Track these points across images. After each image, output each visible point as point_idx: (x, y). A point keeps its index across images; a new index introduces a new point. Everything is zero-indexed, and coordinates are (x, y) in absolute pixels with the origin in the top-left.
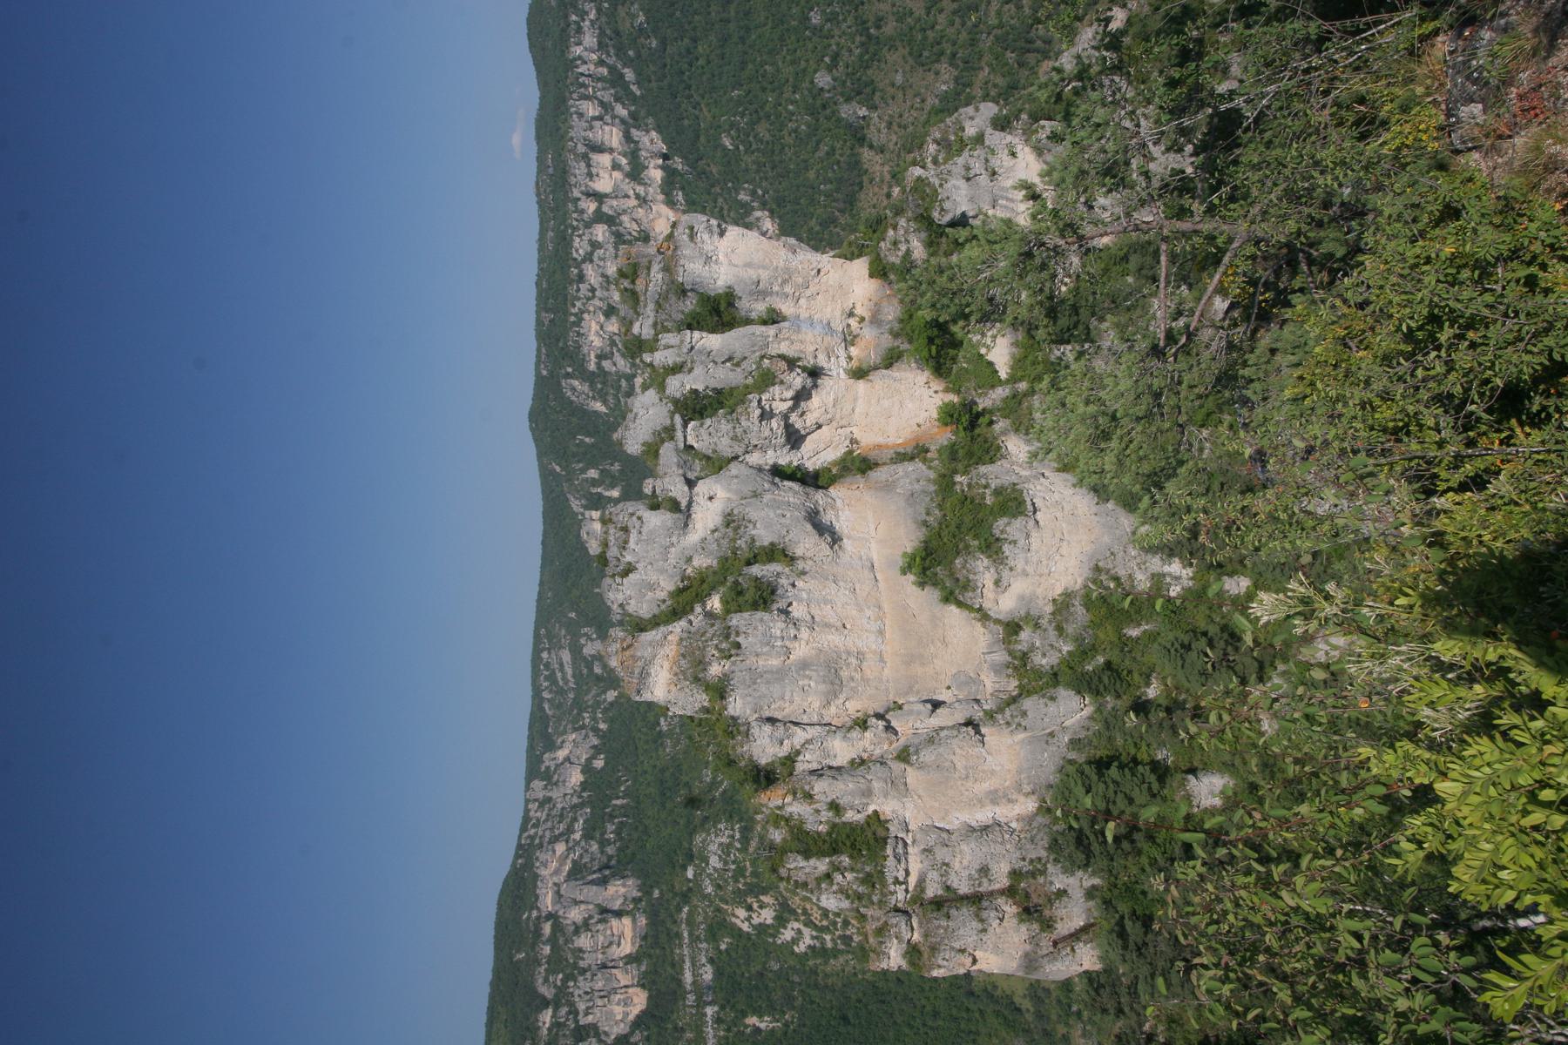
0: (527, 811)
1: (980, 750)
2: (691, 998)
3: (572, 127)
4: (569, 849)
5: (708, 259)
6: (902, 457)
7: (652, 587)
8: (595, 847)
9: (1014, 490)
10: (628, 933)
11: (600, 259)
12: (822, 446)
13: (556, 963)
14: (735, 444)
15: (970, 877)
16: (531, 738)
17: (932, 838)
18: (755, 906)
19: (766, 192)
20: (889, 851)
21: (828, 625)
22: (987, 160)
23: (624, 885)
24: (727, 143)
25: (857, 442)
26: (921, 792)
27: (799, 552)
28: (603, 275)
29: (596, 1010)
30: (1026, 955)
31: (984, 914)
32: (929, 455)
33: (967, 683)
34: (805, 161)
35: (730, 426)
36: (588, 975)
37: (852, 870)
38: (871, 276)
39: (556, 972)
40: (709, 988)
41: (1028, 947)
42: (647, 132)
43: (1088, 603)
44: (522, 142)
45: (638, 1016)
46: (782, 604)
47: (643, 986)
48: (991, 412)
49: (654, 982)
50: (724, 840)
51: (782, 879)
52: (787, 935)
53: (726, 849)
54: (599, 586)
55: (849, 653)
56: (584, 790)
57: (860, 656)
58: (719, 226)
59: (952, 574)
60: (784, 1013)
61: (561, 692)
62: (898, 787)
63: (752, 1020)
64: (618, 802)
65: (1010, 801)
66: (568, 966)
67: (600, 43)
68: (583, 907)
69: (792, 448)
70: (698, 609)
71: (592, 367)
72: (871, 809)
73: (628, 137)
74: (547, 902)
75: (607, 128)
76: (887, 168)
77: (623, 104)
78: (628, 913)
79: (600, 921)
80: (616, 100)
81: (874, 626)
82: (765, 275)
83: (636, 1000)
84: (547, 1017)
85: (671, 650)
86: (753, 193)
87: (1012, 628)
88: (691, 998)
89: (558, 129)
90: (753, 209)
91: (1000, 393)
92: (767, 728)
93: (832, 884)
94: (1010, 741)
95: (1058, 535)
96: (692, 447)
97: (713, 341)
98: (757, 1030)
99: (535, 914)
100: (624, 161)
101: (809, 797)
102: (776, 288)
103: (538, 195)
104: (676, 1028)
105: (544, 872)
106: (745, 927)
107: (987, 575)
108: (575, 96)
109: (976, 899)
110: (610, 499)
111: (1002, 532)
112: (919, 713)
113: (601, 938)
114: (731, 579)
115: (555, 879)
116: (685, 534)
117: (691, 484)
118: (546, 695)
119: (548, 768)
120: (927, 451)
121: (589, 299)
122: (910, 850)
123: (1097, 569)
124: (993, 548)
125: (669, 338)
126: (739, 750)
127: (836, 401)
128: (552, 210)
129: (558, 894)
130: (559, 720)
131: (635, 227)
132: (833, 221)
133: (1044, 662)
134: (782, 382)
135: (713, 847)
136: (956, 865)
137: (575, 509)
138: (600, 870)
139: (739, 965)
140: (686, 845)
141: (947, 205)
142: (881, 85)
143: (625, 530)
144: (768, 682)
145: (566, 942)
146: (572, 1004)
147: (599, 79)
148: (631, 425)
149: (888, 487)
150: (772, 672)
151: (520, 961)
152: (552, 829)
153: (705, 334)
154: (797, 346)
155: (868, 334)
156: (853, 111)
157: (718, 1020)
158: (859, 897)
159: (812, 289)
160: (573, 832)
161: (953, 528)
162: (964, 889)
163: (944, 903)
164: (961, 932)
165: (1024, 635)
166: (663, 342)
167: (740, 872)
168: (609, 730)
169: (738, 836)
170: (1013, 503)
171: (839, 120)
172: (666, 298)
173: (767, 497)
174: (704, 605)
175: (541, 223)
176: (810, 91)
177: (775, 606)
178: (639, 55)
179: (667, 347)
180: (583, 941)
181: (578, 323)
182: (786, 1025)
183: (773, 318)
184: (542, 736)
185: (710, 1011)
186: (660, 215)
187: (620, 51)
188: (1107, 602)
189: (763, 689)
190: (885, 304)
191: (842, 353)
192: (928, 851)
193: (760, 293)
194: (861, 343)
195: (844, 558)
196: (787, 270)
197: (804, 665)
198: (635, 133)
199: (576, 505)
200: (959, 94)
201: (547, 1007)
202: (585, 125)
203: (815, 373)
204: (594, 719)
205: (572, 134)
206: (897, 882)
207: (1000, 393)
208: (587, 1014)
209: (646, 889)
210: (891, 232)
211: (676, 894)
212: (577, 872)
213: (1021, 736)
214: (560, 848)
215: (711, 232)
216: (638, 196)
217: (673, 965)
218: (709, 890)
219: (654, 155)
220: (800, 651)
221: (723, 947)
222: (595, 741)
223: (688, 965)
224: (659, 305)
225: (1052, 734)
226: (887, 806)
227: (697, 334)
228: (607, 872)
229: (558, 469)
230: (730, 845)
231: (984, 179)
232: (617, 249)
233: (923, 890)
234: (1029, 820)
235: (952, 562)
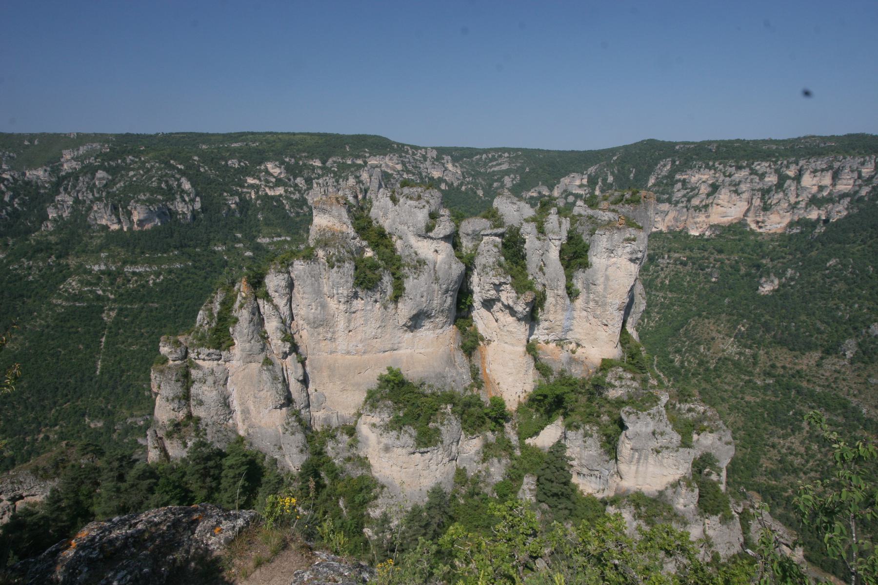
0: (421, 148)
3: (854, 158)
4: (398, 171)
6: (475, 373)
7: (385, 215)
9: (437, 441)
11: (752, 179)
13: (343, 167)
15: (198, 395)
16: (462, 149)
19: (792, 287)
20: (211, 351)
21: (349, 321)
22: (667, 448)
24: (832, 262)
25: (488, 344)
26: (246, 370)
27: (400, 305)
28: (740, 182)
32: (475, 389)
34: (814, 314)
36: (335, 184)
38: (603, 360)
39: (338, 167)
42: (847, 209)
43: (362, 478)
46: (360, 293)
48: (502, 431)
54: (543, 184)
55: (334, 333)
56: (429, 179)
57: (333, 339)
58: (637, 259)
59: (382, 398)
61: (485, 165)
62: (249, 358)
65: (244, 420)
70: (365, 243)
71: (678, 177)
73: (843, 196)
74: (373, 161)
75: (851, 182)
76: (805, 367)
77: (870, 192)
80: (873, 188)
82: (600, 288)
84: (317, 163)
85: (338, 227)
86: (792, 279)
87: (351, 431)
89: (854, 149)
90: (780, 278)
91: (514, 439)
94: (277, 424)
95: (405, 465)
100: (825, 194)
102: (591, 296)
103: (805, 138)
105: (387, 158)
107: (378, 420)
110: (594, 189)
112: (296, 372)
116: (414, 235)
118: (484, 156)
120: (479, 388)
121: (724, 173)
122: (215, 362)
123: (383, 487)
124: (396, 425)
125: (566, 224)
127: (511, 332)
128: (791, 147)
131: (774, 202)
132: (768, 330)
133: (329, 448)
134: (518, 298)
136: (205, 388)
137: (590, 169)
141: (633, 417)
142: (869, 368)
145: (352, 172)
146: (323, 176)
149: (451, 362)
150: (319, 287)
152: (409, 162)
154: (552, 309)
155: (563, 355)
156: (850, 347)
159: (593, 320)
162: (193, 390)
163: (186, 379)
165: (346, 437)
166: (564, 220)
168: (461, 192)
169: (155, 268)
170: (427, 440)
171: (844, 338)
176: (869, 319)
179: (560, 223)
181: (708, 167)
183: (572, 293)
184: (460, 155)
186: (782, 218)
188: (365, 489)
189: (309, 282)
190: (583, 368)
191: (551, 338)
192: (212, 372)
193: (589, 285)
194: (557, 350)
195: (399, 333)
196: (604, 304)
197: (324, 306)
198: (846, 201)
199: (592, 170)
200: (858, 420)
202: (855, 167)
204: (468, 183)
205: (848, 158)
206: (199, 354)
207: (514, 439)
208: (317, 184)
210: (629, 376)
213: (281, 430)
214: (399, 167)
215: (632, 253)
216: (797, 203)
219: (828, 214)
220: (332, 304)
222: (455, 184)
224: (590, 217)
225: (280, 448)
229: (615, 158)
231: (655, 444)
232: (758, 190)
233: (194, 368)
234: (235, 432)
235: (390, 399)
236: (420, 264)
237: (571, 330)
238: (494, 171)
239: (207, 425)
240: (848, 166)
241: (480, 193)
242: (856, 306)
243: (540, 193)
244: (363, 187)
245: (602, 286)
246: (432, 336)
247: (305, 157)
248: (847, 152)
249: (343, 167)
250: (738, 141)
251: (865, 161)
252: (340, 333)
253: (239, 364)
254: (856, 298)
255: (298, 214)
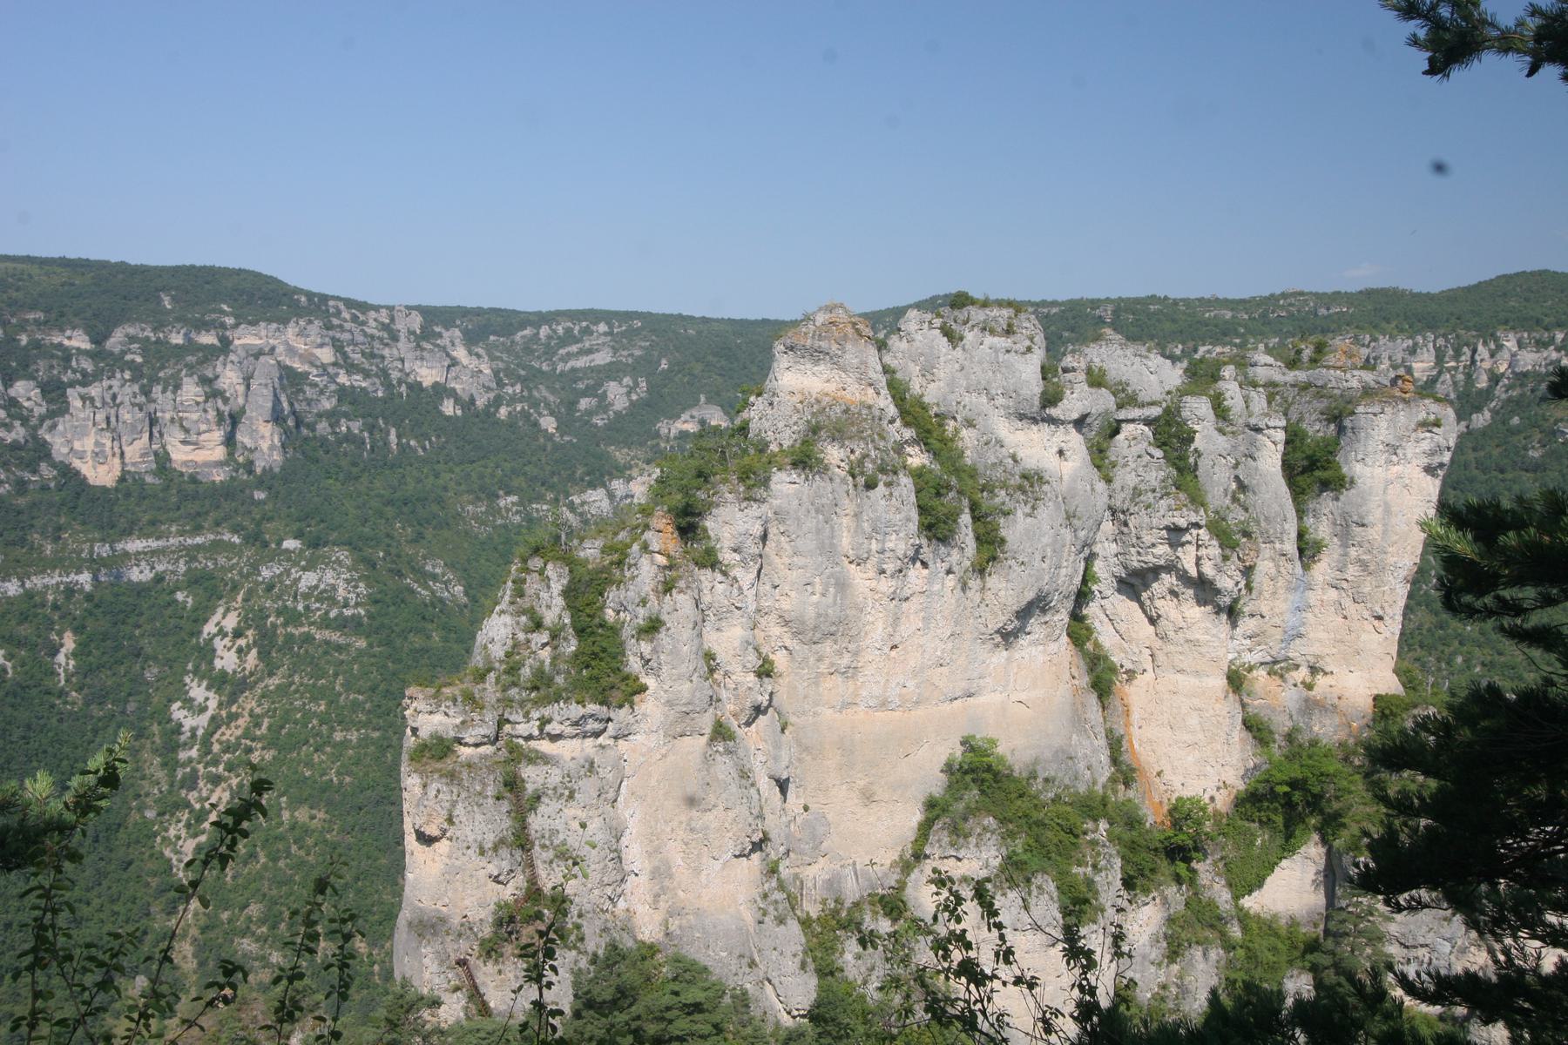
0: (377, 308)
1: (731, 848)
2: (103, 550)
3: (1392, 338)
4: (324, 367)
5: (1393, 449)
6: (1116, 745)
7: (928, 372)
8: (327, 404)
10: (201, 456)
12: (1122, 627)
13: (159, 353)
14: (1128, 493)
15: (556, 832)
16: (479, 312)
17: (607, 773)
18: (242, 642)
20: (592, 708)
21: (896, 620)
23: (272, 448)
26: (671, 758)
27: (993, 581)
29: (89, 412)
30: (443, 920)
31: (504, 852)
33: (814, 838)
35: (1155, 484)
36: (141, 399)
37: (554, 658)
38: (1377, 698)
39: (144, 351)
40: (119, 576)
41: (456, 921)
44: (1358, 274)
45: (77, 473)
46: (926, 553)
47: (122, 479)
48: (1192, 882)
49: (128, 495)
50: (341, 593)
51: (525, 561)
52: (198, 692)
53: (328, 596)
54: (708, 401)
55: (856, 654)
56: (410, 387)
57: (850, 672)
58: (1441, 465)
60: (79, 690)
61: (549, 352)
63: (69, 642)
64: (393, 437)
65: (657, 896)
66: (156, 368)
67: (1525, 375)
68: (241, 389)
69: (1120, 581)
70: (909, 433)
72: (650, 681)
74: (246, 338)
78: (231, 454)
79: (220, 414)
81: (893, 693)
82: (1374, 533)
83: (102, 469)
85: (855, 393)
88: (103, 550)
92: (757, 529)
93: (527, 631)
94: (741, 898)
96: (1116, 431)
97: (1270, 458)
98: (54, 650)
99: (230, 321)
101: (668, 588)
103: (1284, 296)
104: (59, 528)
105: (291, 331)
106: (209, 628)
108: (1441, 342)
109: (521, 841)
111: (1039, 887)
112: (776, 759)
113: (195, 416)
114: (954, 481)
115: (280, 349)
117: (1080, 423)
118: (544, 331)
119: (440, 335)
122: (589, 742)
126: (724, 488)
128: (1264, 316)
129: (258, 354)
130: (508, 351)
133: (848, 957)
134: (1225, 558)
135: (329, 577)
138: (294, 413)
139: (153, 619)
140: (334, 536)
143: (1009, 331)
144: (818, 531)
145: (190, 367)
146: (96, 377)
147: (1469, 376)
148: (1129, 352)
149: (1078, 721)
151: (159, 301)
152: (353, 342)
153: (1281, 447)
157: (70, 591)
158: (513, 670)
160: (349, 373)
161: (1036, 815)
163: (517, 796)
164: (479, 817)
167: (293, 618)
168: (498, 422)
169: (348, 612)
172: (1319, 395)
173: (1067, 534)
174: (914, 442)
175: (1243, 301)
177: (924, 542)
178: (1513, 432)
179: (1247, 400)
180: (191, 390)
182: (62, 694)
183: (1307, 550)
184: (484, 326)
185: (85, 579)
187: (1515, 405)
189: (810, 524)
190: (1337, 720)
193: (1346, 528)
195: (982, 651)
196: (1382, 568)
197: (842, 585)
201: (92, 342)
202: (1398, 358)
203: (1232, 613)
204: (513, 400)
205: (1383, 340)
206: (544, 721)
208: (83, 398)
209: (265, 480)
211: (258, 524)
212: (291, 380)
213: (749, 917)
214: (326, 355)
215: (1432, 453)
217: (153, 523)
218: (266, 573)
220: (861, 580)
221: (180, 596)
223: (154, 544)
224: (1305, 387)
226: (650, 707)
227: (1280, 436)
228: (291, 423)
230: (332, 601)
233: (531, 761)
235: (989, 812)
236: (1032, 482)
237: (1300, 636)
238: (573, 370)
239: (580, 916)
240: (1385, 355)
241: (549, 424)
242: (1459, 659)
243: (702, 422)
244: (226, 409)
245: (1379, 528)
246: (1041, 658)
247: (37, 322)
248: (1375, 327)
249: (159, 353)
250: (1153, 299)
251: (1415, 344)
252: (868, 656)
253: (653, 741)
254: (1456, 643)
255: (21, 486)
